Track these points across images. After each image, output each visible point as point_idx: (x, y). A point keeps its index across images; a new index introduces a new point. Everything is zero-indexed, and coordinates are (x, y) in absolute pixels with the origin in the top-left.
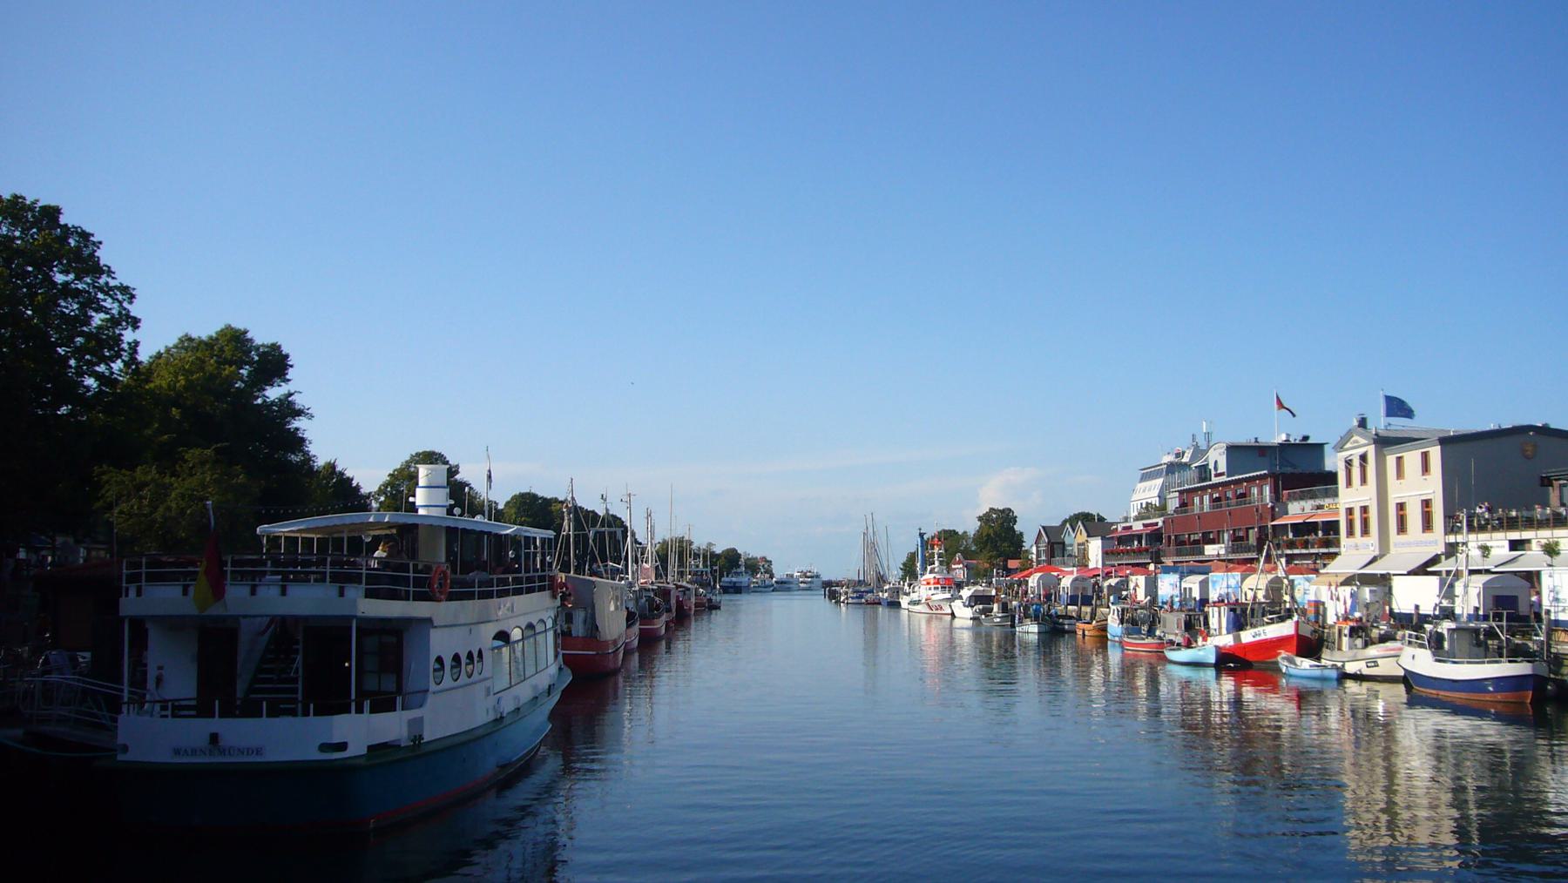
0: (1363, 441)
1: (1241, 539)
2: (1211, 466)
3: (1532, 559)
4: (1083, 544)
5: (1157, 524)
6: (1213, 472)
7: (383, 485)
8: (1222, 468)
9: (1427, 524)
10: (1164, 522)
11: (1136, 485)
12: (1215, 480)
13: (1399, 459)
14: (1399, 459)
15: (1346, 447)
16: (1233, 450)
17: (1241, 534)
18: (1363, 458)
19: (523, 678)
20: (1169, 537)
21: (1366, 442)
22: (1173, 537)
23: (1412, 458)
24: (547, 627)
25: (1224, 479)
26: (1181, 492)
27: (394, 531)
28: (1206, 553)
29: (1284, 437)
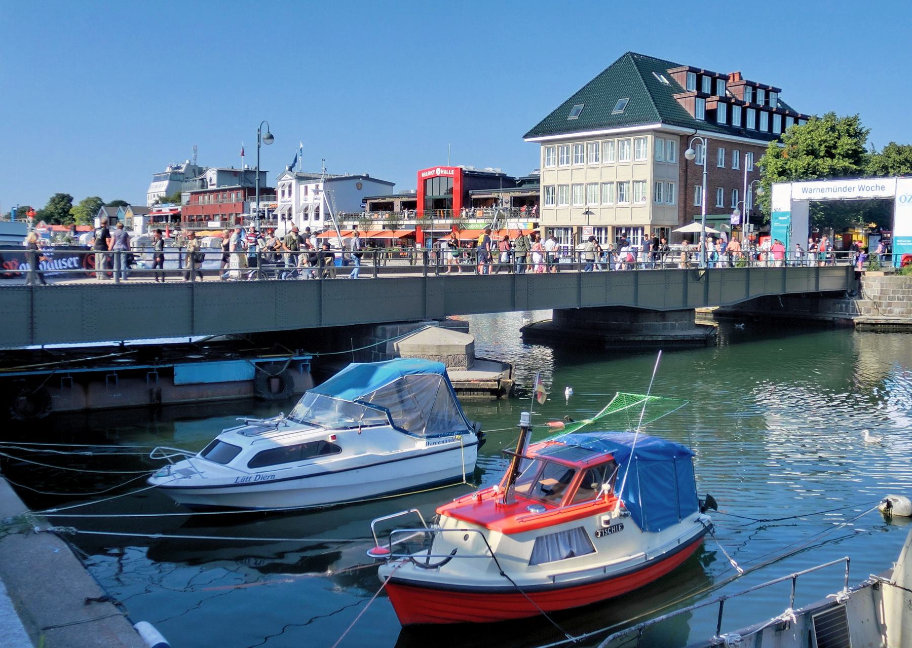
0: (291, 178)
1: (226, 219)
2: (208, 180)
3: (557, 245)
4: (130, 218)
5: (177, 210)
6: (209, 183)
7: (658, 531)
8: (215, 181)
9: (317, 217)
10: (182, 209)
11: (148, 187)
12: (210, 188)
13: (306, 187)
14: (306, 187)
15: (282, 179)
16: (221, 172)
17: (226, 217)
18: (290, 186)
19: (108, 607)
20: (185, 216)
21: (291, 178)
22: (187, 217)
23: (311, 186)
24: (175, 475)
25: (214, 188)
26: (192, 193)
27: (452, 172)
28: (209, 226)
29: (246, 167)
